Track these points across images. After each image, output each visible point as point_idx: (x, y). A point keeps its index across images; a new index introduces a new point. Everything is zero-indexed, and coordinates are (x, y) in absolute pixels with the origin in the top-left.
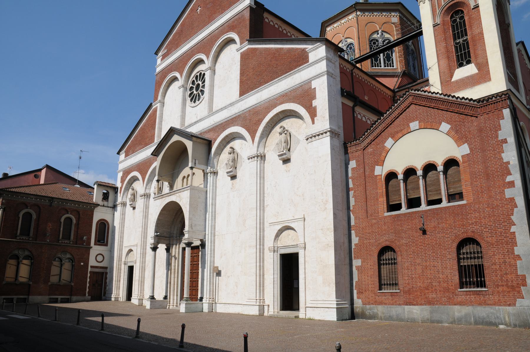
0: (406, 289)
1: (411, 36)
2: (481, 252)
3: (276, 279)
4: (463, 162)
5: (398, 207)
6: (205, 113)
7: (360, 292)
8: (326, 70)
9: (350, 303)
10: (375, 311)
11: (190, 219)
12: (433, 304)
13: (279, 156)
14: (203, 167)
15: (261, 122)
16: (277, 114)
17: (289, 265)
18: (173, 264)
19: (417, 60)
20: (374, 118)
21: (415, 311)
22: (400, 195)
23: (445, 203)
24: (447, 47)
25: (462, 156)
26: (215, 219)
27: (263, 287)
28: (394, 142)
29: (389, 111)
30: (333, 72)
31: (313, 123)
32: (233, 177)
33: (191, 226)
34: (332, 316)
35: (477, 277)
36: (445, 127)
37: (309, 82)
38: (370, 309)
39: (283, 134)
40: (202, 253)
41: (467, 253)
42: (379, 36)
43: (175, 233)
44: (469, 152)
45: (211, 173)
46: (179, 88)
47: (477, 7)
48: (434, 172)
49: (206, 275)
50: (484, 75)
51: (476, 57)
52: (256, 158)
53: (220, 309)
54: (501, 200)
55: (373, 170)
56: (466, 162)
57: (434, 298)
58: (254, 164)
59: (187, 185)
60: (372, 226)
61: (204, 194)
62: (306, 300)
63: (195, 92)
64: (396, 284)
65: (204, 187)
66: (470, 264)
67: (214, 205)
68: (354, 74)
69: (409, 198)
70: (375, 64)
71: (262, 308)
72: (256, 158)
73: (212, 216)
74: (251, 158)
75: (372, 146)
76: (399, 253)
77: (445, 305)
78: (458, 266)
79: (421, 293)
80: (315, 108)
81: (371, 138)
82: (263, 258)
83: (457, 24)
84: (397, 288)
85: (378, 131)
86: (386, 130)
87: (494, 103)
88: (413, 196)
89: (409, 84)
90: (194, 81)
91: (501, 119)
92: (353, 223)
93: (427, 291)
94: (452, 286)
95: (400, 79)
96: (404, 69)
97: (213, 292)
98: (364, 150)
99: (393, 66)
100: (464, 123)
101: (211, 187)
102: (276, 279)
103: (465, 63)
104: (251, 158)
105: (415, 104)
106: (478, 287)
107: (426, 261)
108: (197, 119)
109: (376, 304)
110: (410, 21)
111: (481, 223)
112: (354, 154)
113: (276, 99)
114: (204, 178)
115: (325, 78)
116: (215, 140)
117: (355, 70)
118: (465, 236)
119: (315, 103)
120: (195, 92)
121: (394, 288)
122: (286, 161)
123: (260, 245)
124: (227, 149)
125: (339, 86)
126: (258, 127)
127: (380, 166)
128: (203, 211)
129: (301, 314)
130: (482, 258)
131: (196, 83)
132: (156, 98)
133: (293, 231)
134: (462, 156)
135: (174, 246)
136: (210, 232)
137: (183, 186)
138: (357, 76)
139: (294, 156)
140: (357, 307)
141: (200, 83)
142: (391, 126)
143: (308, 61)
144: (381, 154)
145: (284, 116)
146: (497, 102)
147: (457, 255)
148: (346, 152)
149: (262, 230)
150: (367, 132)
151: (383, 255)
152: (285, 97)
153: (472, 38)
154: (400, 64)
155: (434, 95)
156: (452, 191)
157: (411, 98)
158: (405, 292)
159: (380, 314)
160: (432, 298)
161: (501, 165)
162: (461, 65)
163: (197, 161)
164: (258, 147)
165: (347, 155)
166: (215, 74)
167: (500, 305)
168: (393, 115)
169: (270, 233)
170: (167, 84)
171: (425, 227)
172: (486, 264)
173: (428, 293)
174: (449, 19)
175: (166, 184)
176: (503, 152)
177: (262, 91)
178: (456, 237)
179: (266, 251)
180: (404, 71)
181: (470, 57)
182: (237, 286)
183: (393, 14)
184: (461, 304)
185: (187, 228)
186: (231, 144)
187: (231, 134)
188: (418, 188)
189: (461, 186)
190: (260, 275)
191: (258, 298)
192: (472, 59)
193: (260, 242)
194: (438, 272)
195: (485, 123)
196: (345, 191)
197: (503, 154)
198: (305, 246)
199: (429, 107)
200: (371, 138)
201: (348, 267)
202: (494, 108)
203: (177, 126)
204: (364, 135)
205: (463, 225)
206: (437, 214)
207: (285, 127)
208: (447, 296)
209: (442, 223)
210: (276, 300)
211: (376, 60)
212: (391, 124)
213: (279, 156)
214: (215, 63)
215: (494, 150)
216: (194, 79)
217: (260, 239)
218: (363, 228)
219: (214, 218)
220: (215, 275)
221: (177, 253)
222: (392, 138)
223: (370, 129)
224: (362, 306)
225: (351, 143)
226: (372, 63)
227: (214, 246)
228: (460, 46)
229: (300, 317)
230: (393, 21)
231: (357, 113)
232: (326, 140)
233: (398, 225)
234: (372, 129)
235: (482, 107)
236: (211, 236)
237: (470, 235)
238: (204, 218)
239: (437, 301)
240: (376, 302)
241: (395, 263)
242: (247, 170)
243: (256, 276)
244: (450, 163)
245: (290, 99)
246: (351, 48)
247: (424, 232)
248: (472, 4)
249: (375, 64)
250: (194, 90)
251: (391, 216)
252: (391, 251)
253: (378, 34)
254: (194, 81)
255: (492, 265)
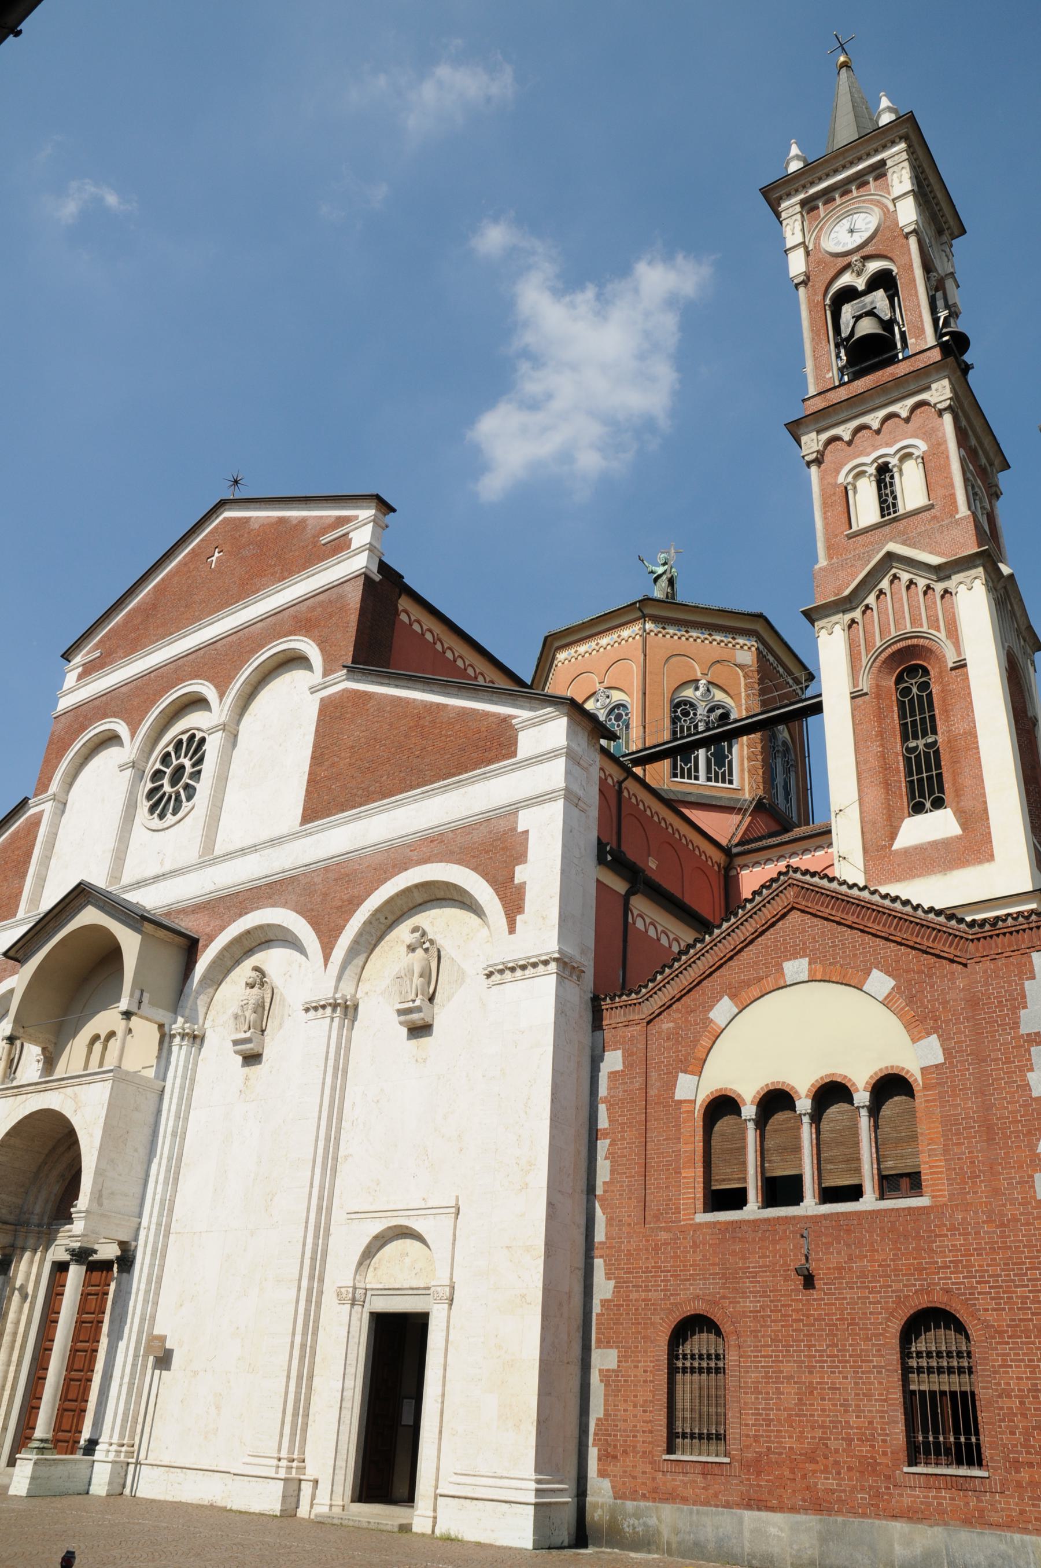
0: (749, 1455)
1: (786, 716)
2: (969, 1354)
3: (348, 1394)
4: (926, 1087)
5: (735, 1199)
6: (192, 855)
7: (608, 1455)
8: (563, 785)
9: (574, 1492)
10: (653, 1521)
11: (99, 1172)
12: (829, 1511)
13: (401, 1012)
14: (163, 1015)
15: (359, 905)
16: (407, 891)
17: (397, 1347)
18: (12, 1316)
19: (797, 773)
20: (687, 935)
21: (773, 1530)
22: (744, 1164)
23: (869, 1201)
24: (883, 756)
25: (922, 1069)
26: (176, 1179)
27: (306, 1415)
28: (736, 1011)
29: (728, 920)
30: (581, 793)
31: (512, 930)
32: (252, 1059)
33: (98, 1196)
34: (517, 1531)
35: (957, 1433)
36: (880, 983)
37: (512, 811)
38: (637, 1515)
39: (420, 952)
40: (118, 1285)
41: (929, 1355)
42: (698, 693)
43: (38, 1209)
44: (940, 1059)
45: (183, 1036)
46: (122, 768)
47: (961, 665)
48: (843, 1106)
49: (121, 1359)
50: (974, 846)
51: (958, 793)
52: (329, 1010)
53: (150, 1486)
54: (1025, 1203)
55: (672, 1086)
56: (932, 1087)
57: (833, 1492)
58: (323, 1028)
59: (101, 1065)
60: (656, 1249)
61: (153, 1097)
62: (438, 1469)
63: (167, 788)
64: (720, 1437)
65: (157, 1077)
66: (936, 1387)
67: (180, 1135)
68: (626, 794)
69: (768, 1175)
70: (682, 769)
71: (292, 1489)
72: (329, 1010)
73: (168, 1170)
74: (316, 1009)
75: (673, 1013)
76: (732, 1340)
77: (864, 1515)
78: (904, 1392)
79: (792, 1471)
80: (521, 889)
81: (672, 990)
82: (317, 1321)
83: (911, 701)
84: (722, 1448)
85: (692, 974)
86: (717, 974)
87: (1011, 933)
88: (780, 1170)
89: (771, 835)
90: (168, 755)
91: (1028, 979)
92: (600, 1236)
93: (810, 1467)
94: (885, 1453)
95: (748, 819)
96: (760, 793)
97: (137, 1421)
98: (648, 1023)
99: (731, 782)
100: (930, 977)
101: (178, 1081)
102: (348, 1394)
103: (928, 805)
104: (316, 1009)
105: (803, 911)
106: (959, 1463)
107: (811, 1369)
108: (165, 868)
109: (654, 1500)
110: (790, 673)
111: (969, 1266)
112: (620, 1032)
113: (408, 845)
114: (160, 1049)
115: (557, 808)
116: (211, 939)
117: (630, 785)
118: (924, 1302)
119: (521, 874)
120: (169, 786)
121: (713, 1448)
122: (420, 1030)
123: (311, 1278)
124: (244, 971)
125: (594, 835)
126: (348, 921)
127: (692, 1073)
128: (142, 1152)
129: (420, 1517)
130: (970, 1372)
131: (175, 762)
132: (43, 786)
133: (417, 1244)
134: (922, 1069)
135: (27, 1255)
136: (154, 1220)
137: (86, 1068)
138: (634, 800)
139: (442, 1018)
140: (595, 1506)
141: (187, 763)
142: (731, 963)
143: (514, 754)
144: (696, 1041)
145: (426, 897)
146: (1018, 932)
147: (902, 1358)
148: (597, 1024)
149: (322, 1231)
150: (662, 973)
151: (685, 1340)
152: (437, 845)
153: (949, 742)
154: (750, 777)
155: (855, 892)
156: (891, 1166)
157: (791, 893)
158: (745, 1465)
159: (666, 1534)
160: (827, 1491)
161: (1026, 1105)
162: (918, 809)
163: (146, 997)
164: (339, 978)
165: (598, 1033)
166: (234, 744)
167: (1025, 1531)
168: (740, 935)
169: (347, 1242)
170: (85, 751)
171: (812, 1266)
172: (981, 1393)
173: (814, 1472)
174: (892, 683)
175: (32, 1052)
176: (1032, 1070)
177: (370, 816)
178: (898, 1302)
179: (329, 1298)
180: (760, 799)
181: (941, 790)
182: (218, 1408)
183: (741, 641)
184: (910, 1515)
185: (83, 1201)
186: (258, 959)
187: (261, 927)
188: (797, 1149)
189: (916, 1154)
190: (300, 1377)
191: (284, 1454)
192: (948, 796)
193: (313, 1268)
194: (846, 1406)
195: (987, 984)
196: (586, 1136)
197: (1030, 1075)
198: (452, 1293)
199: (839, 923)
200: (672, 990)
201: (575, 1370)
202: (1010, 944)
203: (99, 880)
204: (653, 980)
205: (920, 1269)
206: (848, 1231)
207: (427, 929)
208: (871, 1487)
209: (862, 1257)
210: (341, 1463)
211: (686, 761)
212: (731, 958)
213: (401, 1012)
214: (241, 715)
215: (1008, 1061)
216: (170, 749)
217: (313, 1259)
218: (629, 1254)
219: (174, 1177)
220: (150, 1364)
221: (33, 1277)
222: (733, 997)
223: (670, 967)
224: (612, 1500)
225: (612, 999)
226: (675, 767)
227: (162, 1267)
228: (918, 757)
229: (415, 1529)
230: (739, 661)
231: (636, 912)
232: (545, 987)
233: (733, 1253)
234: (676, 965)
235: (978, 939)
236: (157, 1235)
237: (938, 1300)
238: (142, 1175)
239: (840, 1500)
240: (655, 1490)
241: (718, 1370)
242: (298, 1041)
243: (288, 1377)
244: (891, 1086)
245: (452, 852)
246: (619, 717)
247: (809, 1281)
248: (951, 659)
249: (682, 769)
250: (166, 781)
251: (715, 1223)
252: (709, 1332)
253: (697, 689)
254: (168, 755)
255: (1000, 1396)
